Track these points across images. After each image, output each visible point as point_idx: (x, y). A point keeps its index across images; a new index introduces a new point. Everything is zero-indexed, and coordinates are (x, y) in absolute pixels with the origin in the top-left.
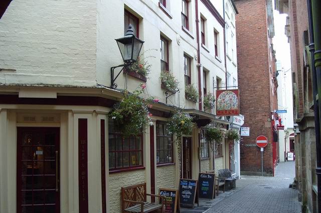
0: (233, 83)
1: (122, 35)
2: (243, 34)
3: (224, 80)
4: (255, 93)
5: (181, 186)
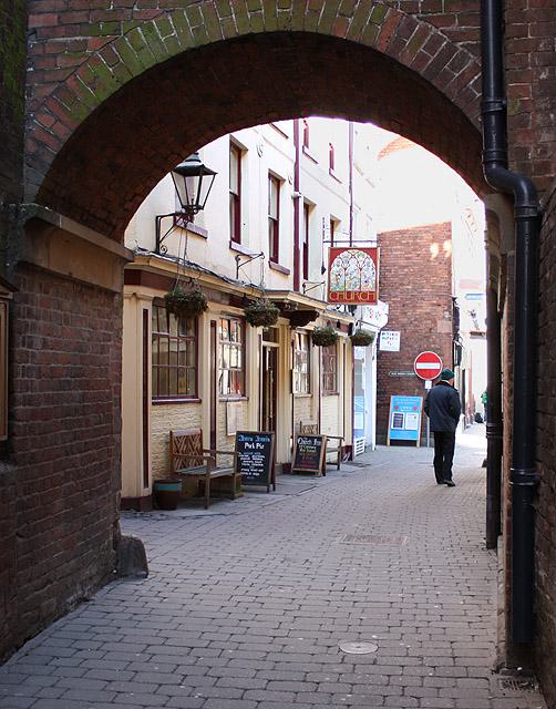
3: (344, 224)
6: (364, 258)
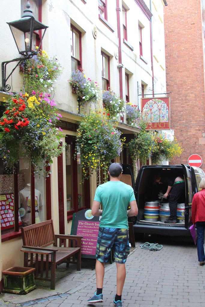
0: (161, 89)
1: (17, 17)
2: (173, 31)
3: (150, 86)
4: (186, 102)
6: (162, 103)
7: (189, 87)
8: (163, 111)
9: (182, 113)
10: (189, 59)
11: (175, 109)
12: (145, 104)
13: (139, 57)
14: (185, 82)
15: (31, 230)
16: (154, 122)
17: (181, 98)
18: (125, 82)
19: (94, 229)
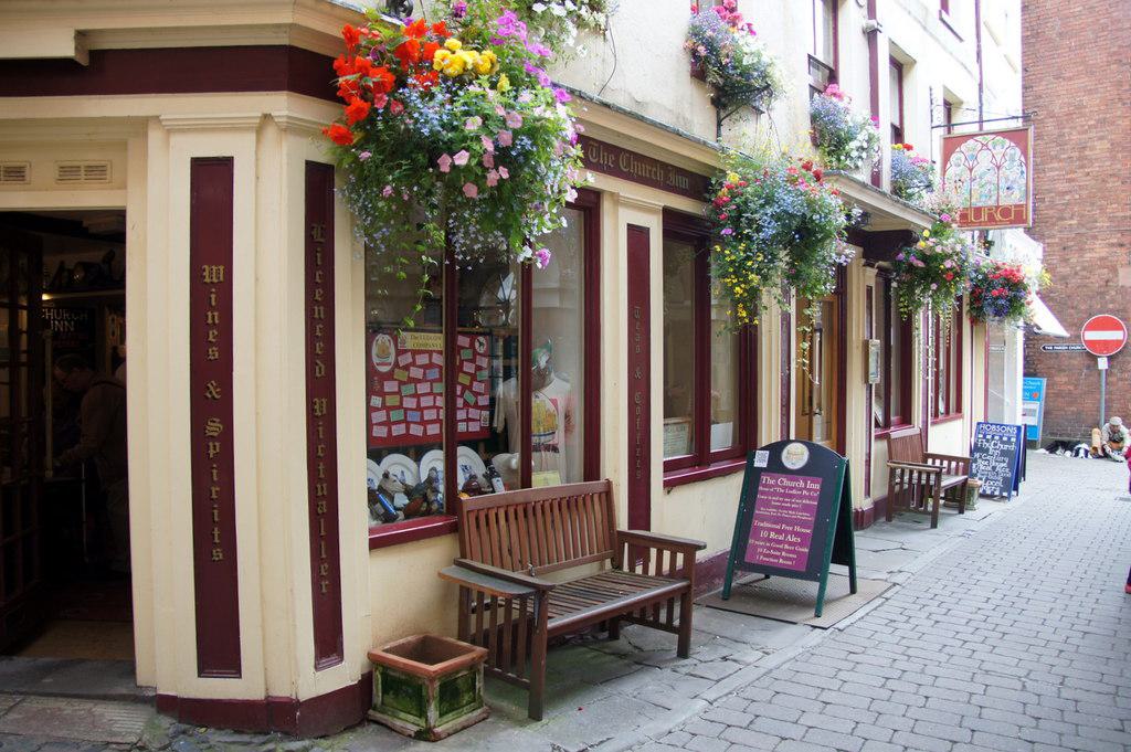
0: (1006, 101)
4: (1082, 167)
5: (662, 544)
7: (1092, 122)
8: (1008, 172)
9: (1067, 197)
10: (1097, 37)
11: (1047, 187)
12: (954, 152)
13: (936, 15)
14: (1080, 107)
15: (592, 496)
16: (980, 205)
17: (1065, 156)
18: (888, 70)
19: (805, 497)
